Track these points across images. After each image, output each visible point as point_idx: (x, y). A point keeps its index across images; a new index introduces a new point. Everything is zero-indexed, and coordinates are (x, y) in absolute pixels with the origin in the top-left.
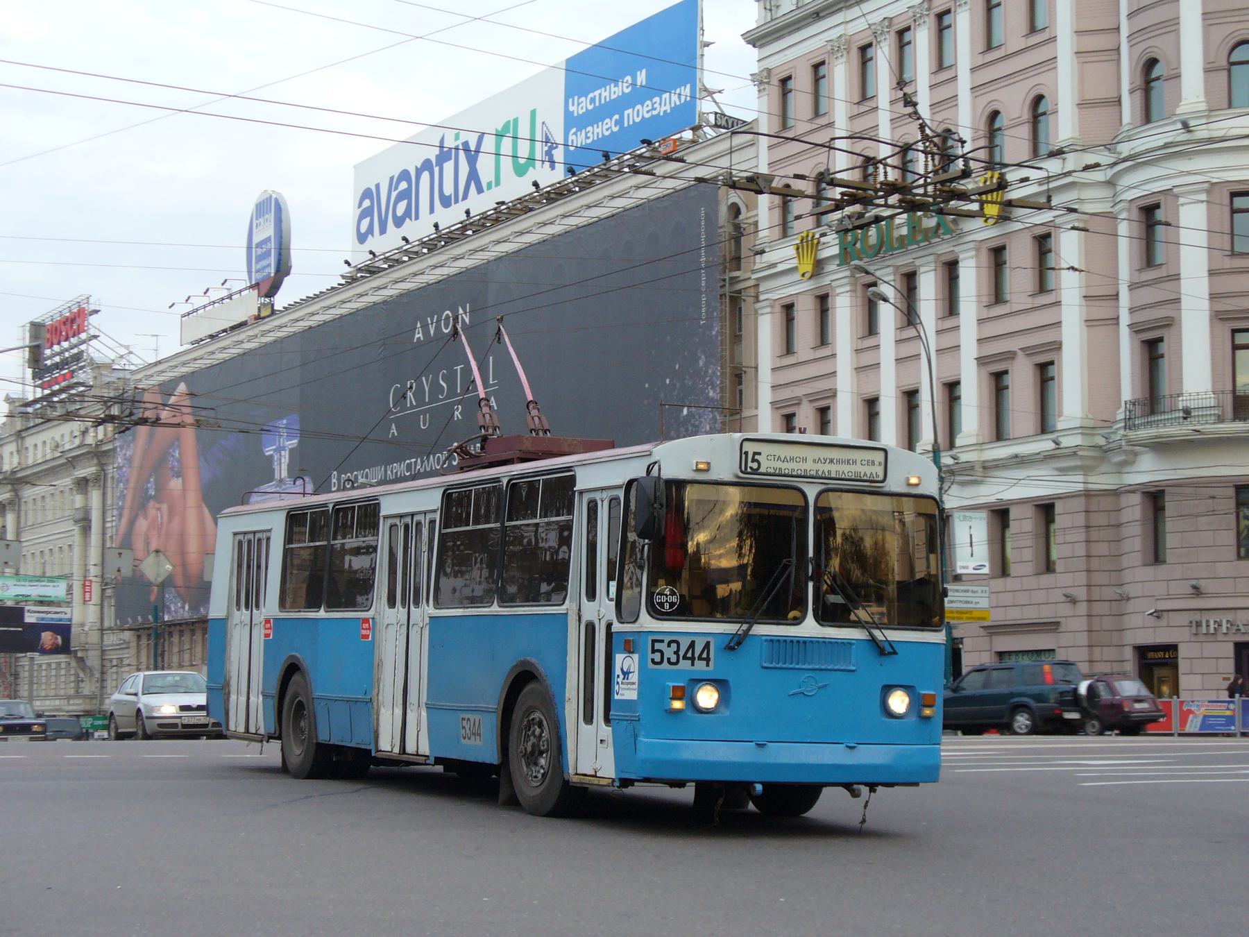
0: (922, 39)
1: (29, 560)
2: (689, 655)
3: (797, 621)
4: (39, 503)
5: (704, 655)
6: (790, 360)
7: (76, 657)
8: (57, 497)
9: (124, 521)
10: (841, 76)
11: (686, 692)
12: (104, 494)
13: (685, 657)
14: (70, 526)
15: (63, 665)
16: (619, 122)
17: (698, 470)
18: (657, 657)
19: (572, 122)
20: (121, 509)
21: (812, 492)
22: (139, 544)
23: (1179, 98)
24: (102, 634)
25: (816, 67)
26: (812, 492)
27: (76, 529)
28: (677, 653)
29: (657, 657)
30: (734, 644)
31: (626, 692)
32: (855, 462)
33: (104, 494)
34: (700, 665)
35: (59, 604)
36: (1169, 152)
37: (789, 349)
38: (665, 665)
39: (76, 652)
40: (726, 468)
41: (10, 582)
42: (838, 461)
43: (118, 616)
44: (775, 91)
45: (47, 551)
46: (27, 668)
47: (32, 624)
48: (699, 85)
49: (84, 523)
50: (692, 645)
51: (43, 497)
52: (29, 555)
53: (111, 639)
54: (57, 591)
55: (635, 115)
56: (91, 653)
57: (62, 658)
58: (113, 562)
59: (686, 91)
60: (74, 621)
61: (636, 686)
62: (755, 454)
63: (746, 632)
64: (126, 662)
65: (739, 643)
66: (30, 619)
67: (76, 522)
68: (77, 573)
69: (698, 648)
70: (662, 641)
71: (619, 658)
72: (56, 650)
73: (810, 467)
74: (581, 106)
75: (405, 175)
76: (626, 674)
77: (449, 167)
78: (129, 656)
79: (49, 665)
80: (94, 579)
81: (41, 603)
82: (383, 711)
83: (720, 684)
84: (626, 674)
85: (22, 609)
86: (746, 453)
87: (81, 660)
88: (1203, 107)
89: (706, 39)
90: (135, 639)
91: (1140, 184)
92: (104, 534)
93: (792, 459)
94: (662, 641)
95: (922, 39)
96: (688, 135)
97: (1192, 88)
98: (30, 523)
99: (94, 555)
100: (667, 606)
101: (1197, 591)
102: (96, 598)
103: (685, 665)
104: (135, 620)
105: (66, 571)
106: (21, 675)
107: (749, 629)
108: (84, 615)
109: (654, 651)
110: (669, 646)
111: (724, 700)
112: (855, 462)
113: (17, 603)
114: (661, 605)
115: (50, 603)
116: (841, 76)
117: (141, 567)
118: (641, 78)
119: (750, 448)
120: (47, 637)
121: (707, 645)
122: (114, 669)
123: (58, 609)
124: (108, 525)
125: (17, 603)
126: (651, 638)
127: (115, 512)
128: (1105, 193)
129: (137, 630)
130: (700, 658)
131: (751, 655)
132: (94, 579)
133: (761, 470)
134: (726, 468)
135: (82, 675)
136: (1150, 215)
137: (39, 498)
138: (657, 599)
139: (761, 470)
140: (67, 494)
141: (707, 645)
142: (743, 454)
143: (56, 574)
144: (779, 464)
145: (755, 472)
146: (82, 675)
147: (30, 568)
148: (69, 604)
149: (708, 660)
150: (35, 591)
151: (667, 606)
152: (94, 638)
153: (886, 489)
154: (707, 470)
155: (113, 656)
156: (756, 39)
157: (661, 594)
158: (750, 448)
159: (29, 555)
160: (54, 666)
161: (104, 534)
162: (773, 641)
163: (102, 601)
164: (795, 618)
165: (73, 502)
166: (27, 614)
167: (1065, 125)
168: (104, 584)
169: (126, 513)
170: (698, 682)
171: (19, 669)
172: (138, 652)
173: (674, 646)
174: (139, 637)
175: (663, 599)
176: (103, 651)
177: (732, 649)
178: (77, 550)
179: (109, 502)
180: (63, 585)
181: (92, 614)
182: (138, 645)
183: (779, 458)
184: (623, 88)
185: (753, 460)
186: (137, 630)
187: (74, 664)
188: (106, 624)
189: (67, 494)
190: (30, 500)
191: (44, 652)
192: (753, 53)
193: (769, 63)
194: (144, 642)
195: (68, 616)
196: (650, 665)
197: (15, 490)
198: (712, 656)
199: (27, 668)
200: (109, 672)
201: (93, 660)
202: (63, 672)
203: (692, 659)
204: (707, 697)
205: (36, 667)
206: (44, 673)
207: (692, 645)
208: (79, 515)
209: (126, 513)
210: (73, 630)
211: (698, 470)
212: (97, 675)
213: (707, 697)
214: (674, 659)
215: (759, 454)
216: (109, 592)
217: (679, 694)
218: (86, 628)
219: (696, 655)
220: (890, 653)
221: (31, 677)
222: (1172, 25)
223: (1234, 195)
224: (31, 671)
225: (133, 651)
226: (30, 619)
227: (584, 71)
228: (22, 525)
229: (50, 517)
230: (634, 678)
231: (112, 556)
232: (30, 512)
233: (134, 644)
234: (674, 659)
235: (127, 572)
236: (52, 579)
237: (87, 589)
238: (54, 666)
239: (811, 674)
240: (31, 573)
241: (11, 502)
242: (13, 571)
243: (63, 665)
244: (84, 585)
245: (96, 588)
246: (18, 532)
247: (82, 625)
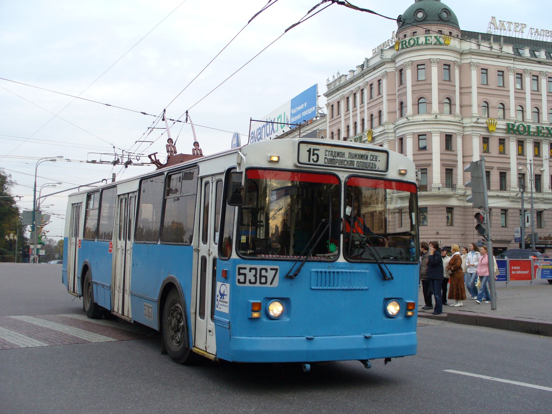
0: (358, 96)
6: (333, 119)
10: (343, 105)
16: (301, 116)
18: (242, 278)
19: (293, 115)
23: (407, 112)
25: (339, 102)
29: (242, 278)
31: (223, 308)
36: (404, 125)
37: (332, 117)
44: (330, 107)
48: (317, 106)
55: (305, 113)
59: (314, 108)
61: (228, 305)
62: (314, 150)
70: (245, 268)
71: (219, 284)
74: (294, 111)
75: (260, 129)
76: (222, 295)
77: (268, 126)
83: (284, 301)
84: (222, 295)
88: (412, 114)
89: (319, 95)
91: (400, 133)
94: (245, 268)
95: (358, 96)
96: (315, 119)
97: (409, 109)
101: (437, 233)
109: (240, 274)
110: (250, 271)
111: (287, 311)
116: (343, 105)
118: (306, 104)
128: (393, 135)
136: (401, 139)
156: (327, 95)
167: (385, 118)
173: (253, 271)
177: (291, 278)
184: (302, 107)
192: (326, 98)
193: (330, 101)
213: (276, 309)
214: (253, 280)
215: (318, 150)
217: (256, 308)
220: (389, 279)
222: (405, 93)
223: (419, 136)
227: (295, 102)
228: (37, 197)
230: (227, 299)
234: (253, 280)
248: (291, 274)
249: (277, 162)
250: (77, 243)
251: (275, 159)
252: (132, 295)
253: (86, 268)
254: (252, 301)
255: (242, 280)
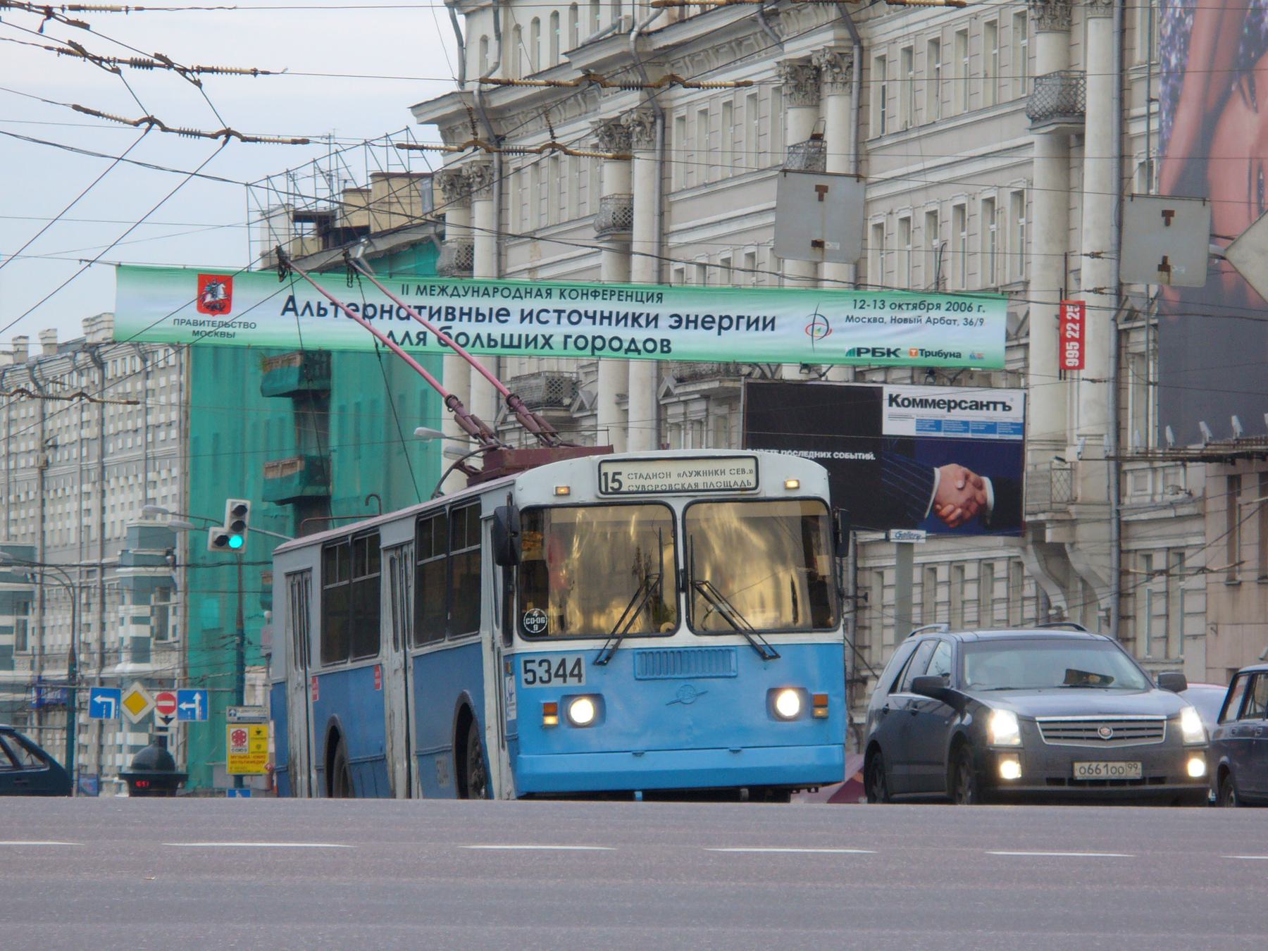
1: (895, 239)
2: (561, 672)
3: (671, 633)
4: (922, 61)
5: (576, 672)
7: (1039, 542)
8: (980, 43)
9: (1186, 116)
11: (560, 708)
12: (1123, 32)
13: (557, 675)
14: (1016, 131)
15: (1000, 569)
17: (558, 495)
20: (1176, 76)
21: (678, 506)
22: (1232, 183)
24: (1120, 475)
26: (678, 506)
27: (1038, 144)
28: (548, 671)
29: (530, 677)
30: (603, 660)
32: (723, 472)
33: (1123, 32)
34: (572, 681)
35: (985, 378)
38: (538, 684)
39: (1040, 527)
40: (586, 491)
41: (835, 312)
42: (705, 473)
43: (1167, 415)
45: (948, 213)
46: (890, 577)
47: (904, 443)
49: (1064, 124)
50: (563, 663)
51: (936, 43)
52: (894, 226)
53: (1146, 488)
54: (979, 336)
56: (1083, 531)
57: (997, 547)
58: (1150, 240)
60: (1033, 431)
62: (615, 474)
63: (616, 648)
64: (1194, 560)
65: (608, 658)
66: (897, 423)
67: (1036, 119)
68: (1042, 284)
69: (569, 666)
72: (976, 522)
73: (675, 482)
78: (1204, 542)
79: (959, 567)
80: (1090, 299)
81: (932, 375)
82: (487, 732)
83: (597, 698)
85: (876, 394)
86: (606, 474)
87: (1057, 553)
90: (1221, 487)
92: (1123, 157)
93: (655, 476)
98: (895, 125)
99: (1092, 227)
100: (536, 627)
102: (1098, 359)
103: (557, 682)
104: (1221, 430)
105: (1007, 276)
106: (874, 597)
107: (618, 643)
108: (1064, 415)
109: (527, 671)
110: (540, 664)
112: (723, 472)
113: (859, 375)
114: (531, 626)
115: (959, 376)
117: (1234, 255)
119: (609, 469)
120: (949, 481)
121: (578, 662)
122: (1159, 583)
123: (984, 395)
124: (1137, 128)
125: (859, 375)
126: (523, 659)
127: (1158, 88)
129: (1227, 460)
130: (572, 675)
131: (623, 667)
132: (1090, 299)
133: (623, 489)
134: (586, 491)
135: (1058, 599)
137: (923, 46)
138: (527, 621)
139: (623, 489)
140: (1008, 33)
141: (578, 662)
142: (601, 475)
143: (977, 283)
144: (641, 482)
145: (616, 491)
146: (1058, 599)
147: (896, 265)
148: (1017, 377)
149: (579, 676)
150: (912, 337)
151: (536, 627)
152: (1094, 484)
153: (762, 496)
154: (568, 494)
155: (1154, 541)
157: (530, 616)
158: (609, 469)
159: (894, 226)
160: (971, 571)
161: (1123, 157)
162: (643, 653)
163: (1119, 367)
164: (668, 630)
165: (1028, 56)
166: (887, 410)
168: (1125, 314)
169: (1192, 87)
170: (570, 697)
171: (869, 579)
172: (1233, 530)
173: (545, 665)
174: (1234, 483)
175: (532, 621)
176: (1122, 527)
177: (601, 663)
178: (1040, 206)
179: (1139, 55)
180: (995, 319)
181: (1087, 409)
182: (1232, 509)
183: (641, 476)
185: (614, 480)
186: (1232, 459)
187: (1032, 564)
188: (1133, 441)
189: (1008, 33)
190: (896, 54)
191: (941, 527)
194: (1251, 497)
195: (1015, 415)
196: (525, 685)
197: (848, 23)
198: (583, 671)
199: (890, 577)
200: (1142, 592)
201: (1092, 552)
202: (1000, 590)
203: (564, 676)
204: (582, 711)
205: (917, 575)
206: (942, 594)
207: (563, 663)
208: (1047, 99)
209: (1192, 87)
210: (1031, 457)
211: (558, 495)
212: (1106, 600)
213: (582, 711)
214: (545, 677)
215: (620, 473)
216: (1139, 341)
217: (551, 710)
218: (1071, 454)
219: (568, 672)
221: (904, 601)
224: (904, 584)
225: (1216, 525)
226: (897, 423)
229: (955, 107)
231: (1143, 216)
232: (895, 90)
233: (1217, 504)
234: (545, 677)
235: (1189, 269)
236: (962, 300)
237: (1071, 330)
238: (971, 571)
239: (683, 683)
240: (899, 280)
241: (838, 61)
242: (846, 272)
243: (1000, 569)
244: (1062, 318)
245: (1099, 330)
246: (860, 157)
247: (1059, 443)
248: (602, 658)
249: (798, 488)
250: (310, 682)
251: (792, 484)
252: (420, 756)
253: (334, 737)
254: (543, 702)
255: (531, 679)
